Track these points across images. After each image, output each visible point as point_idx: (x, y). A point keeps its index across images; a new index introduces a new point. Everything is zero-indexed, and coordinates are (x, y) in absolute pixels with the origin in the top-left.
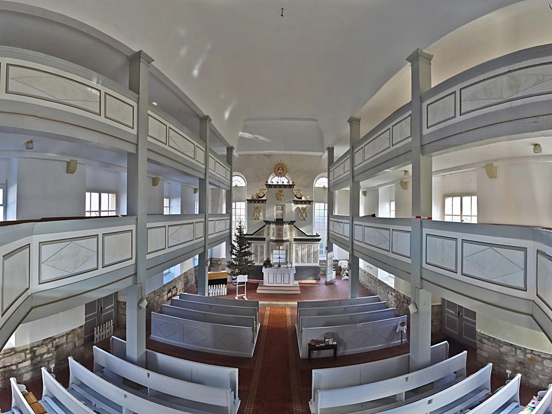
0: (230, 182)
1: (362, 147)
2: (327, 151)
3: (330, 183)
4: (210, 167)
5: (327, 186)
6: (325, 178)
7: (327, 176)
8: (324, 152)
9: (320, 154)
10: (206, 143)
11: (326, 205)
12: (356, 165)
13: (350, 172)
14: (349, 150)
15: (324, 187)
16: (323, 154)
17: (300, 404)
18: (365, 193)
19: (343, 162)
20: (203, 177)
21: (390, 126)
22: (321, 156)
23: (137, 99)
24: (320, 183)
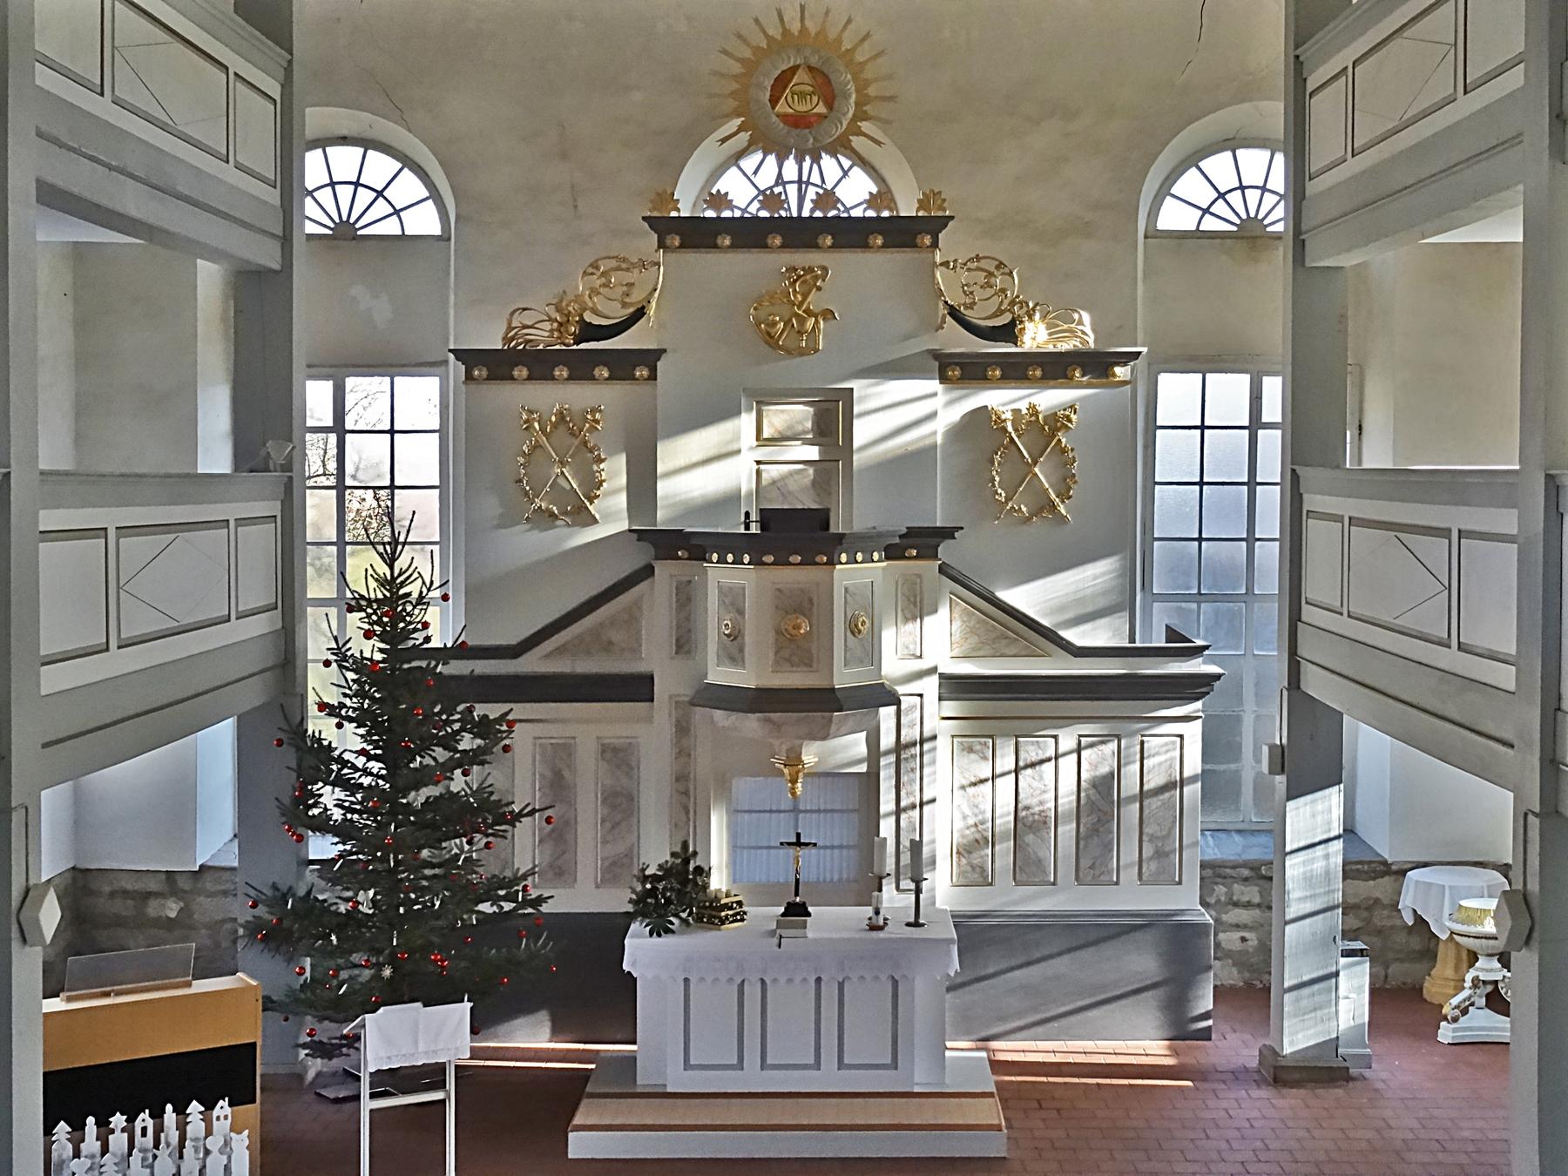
24: (1205, 196)
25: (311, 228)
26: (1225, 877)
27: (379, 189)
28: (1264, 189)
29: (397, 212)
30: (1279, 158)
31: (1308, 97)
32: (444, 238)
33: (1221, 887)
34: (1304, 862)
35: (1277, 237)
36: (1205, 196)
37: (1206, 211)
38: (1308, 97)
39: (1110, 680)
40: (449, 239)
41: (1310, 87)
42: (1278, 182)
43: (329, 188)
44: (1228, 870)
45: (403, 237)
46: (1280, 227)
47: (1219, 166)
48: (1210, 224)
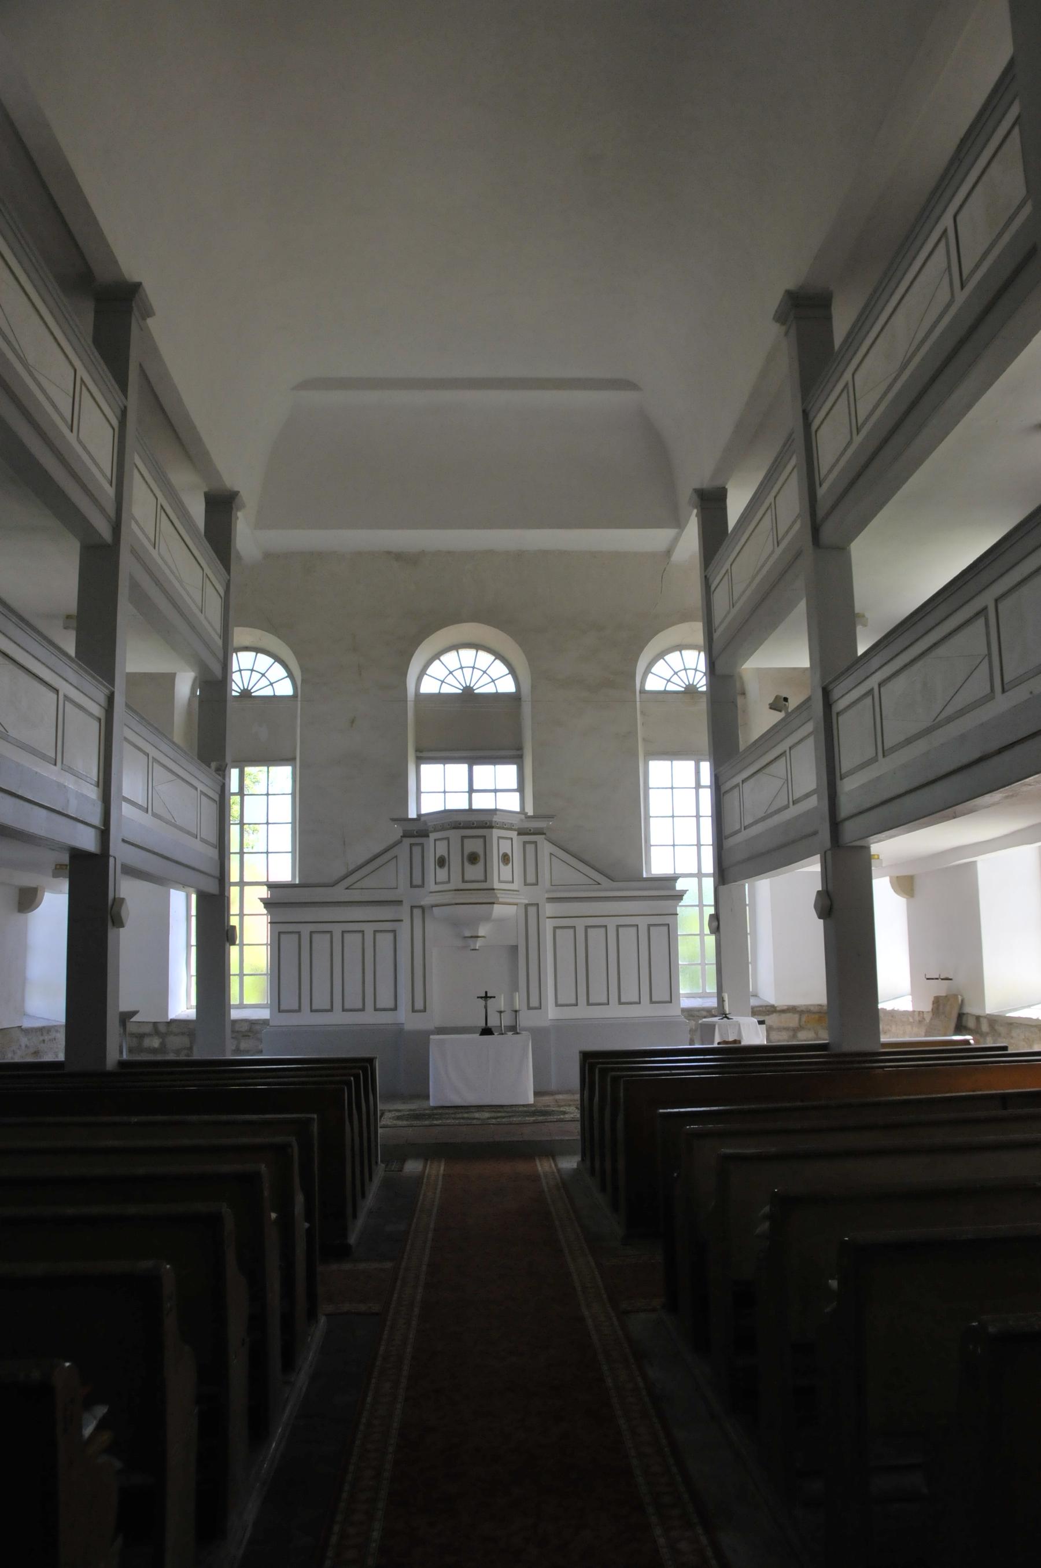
0: (214, 853)
1: (870, 692)
2: (695, 511)
3: (729, 843)
4: (126, 793)
5: (702, 685)
6: (695, 653)
7: (700, 638)
8: (679, 523)
9: (655, 538)
10: (113, 685)
11: (706, 767)
12: (843, 771)
13: (819, 799)
14: (809, 699)
15: (690, 691)
16: (676, 540)
17: (700, 1530)
18: (905, 885)
19: (783, 754)
20: (87, 841)
21: (987, 599)
22: (669, 553)
23: (217, 881)
24: (668, 674)
25: (234, 693)
26: (694, 1016)
27: (263, 673)
28: (696, 670)
29: (263, 675)
30: (702, 654)
31: (722, 795)
32: (294, 696)
33: (692, 1021)
34: (553, 1172)
35: (702, 692)
36: (668, 674)
37: (669, 681)
38: (722, 795)
39: (510, 814)
40: (297, 697)
41: (723, 791)
42: (702, 666)
43: (239, 672)
44: (695, 1013)
45: (275, 696)
46: (704, 689)
47: (673, 658)
48: (671, 687)
